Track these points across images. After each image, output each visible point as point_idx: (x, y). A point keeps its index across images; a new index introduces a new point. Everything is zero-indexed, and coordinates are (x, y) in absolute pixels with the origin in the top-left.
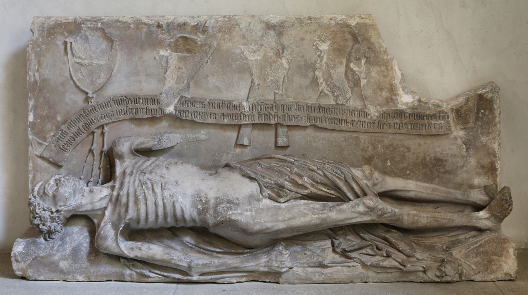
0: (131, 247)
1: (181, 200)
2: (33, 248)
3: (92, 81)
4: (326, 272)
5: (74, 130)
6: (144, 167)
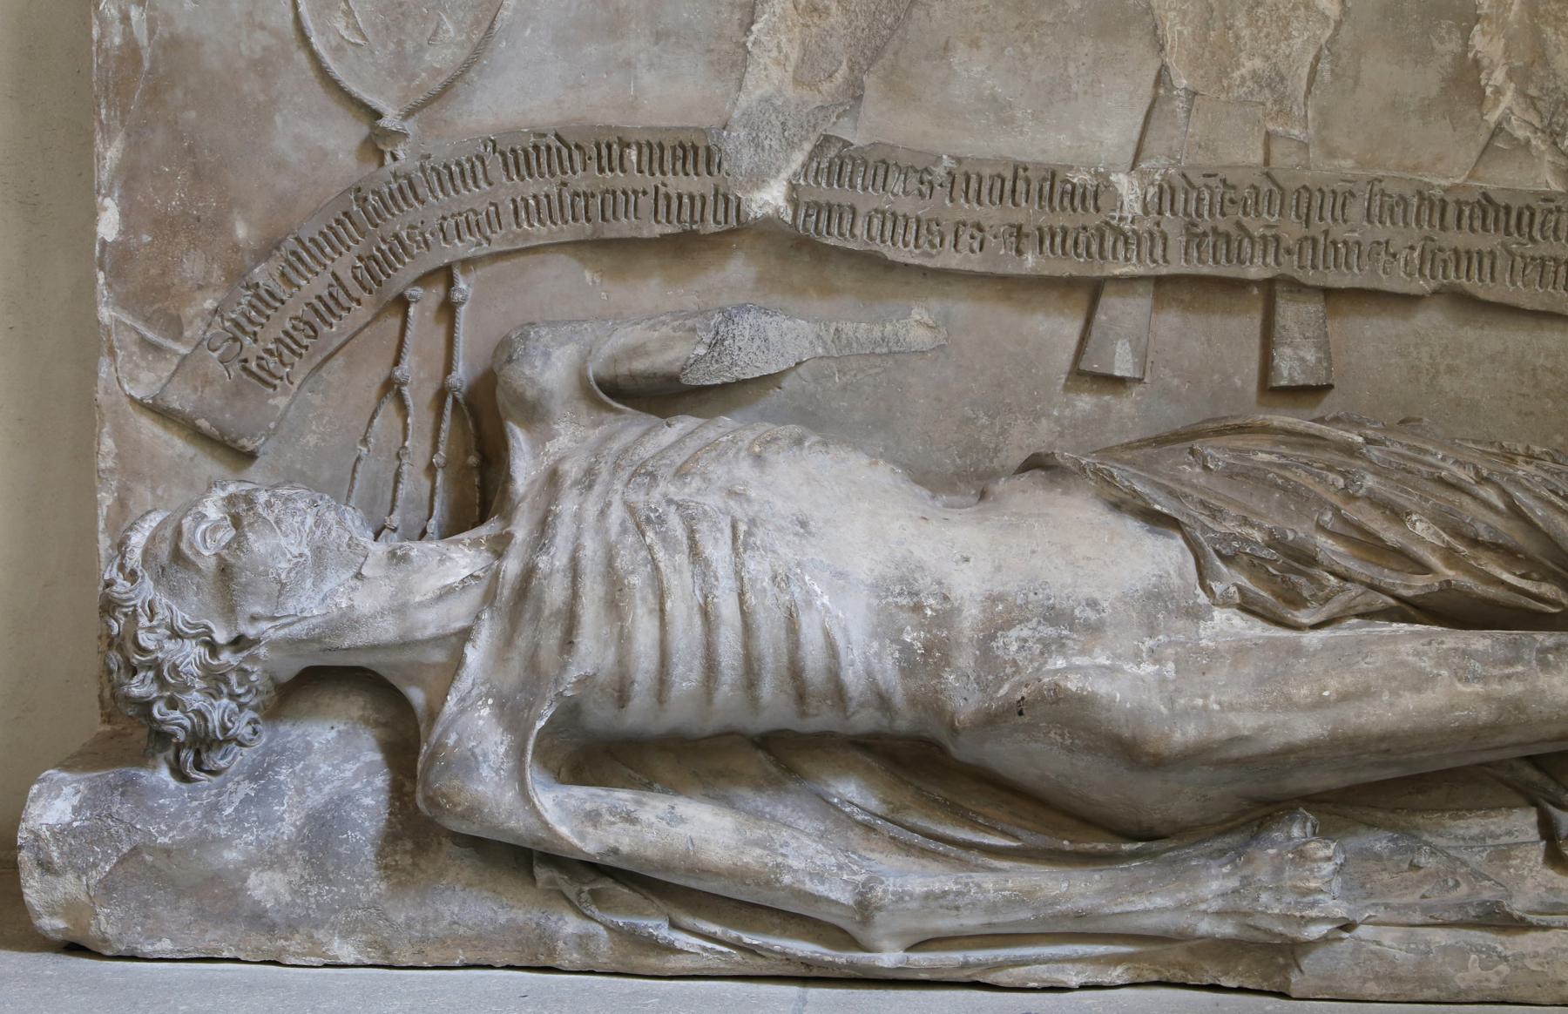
0: (588, 806)
1: (826, 599)
2: (122, 808)
3: (400, 55)
4: (1518, 949)
5: (315, 286)
6: (648, 450)
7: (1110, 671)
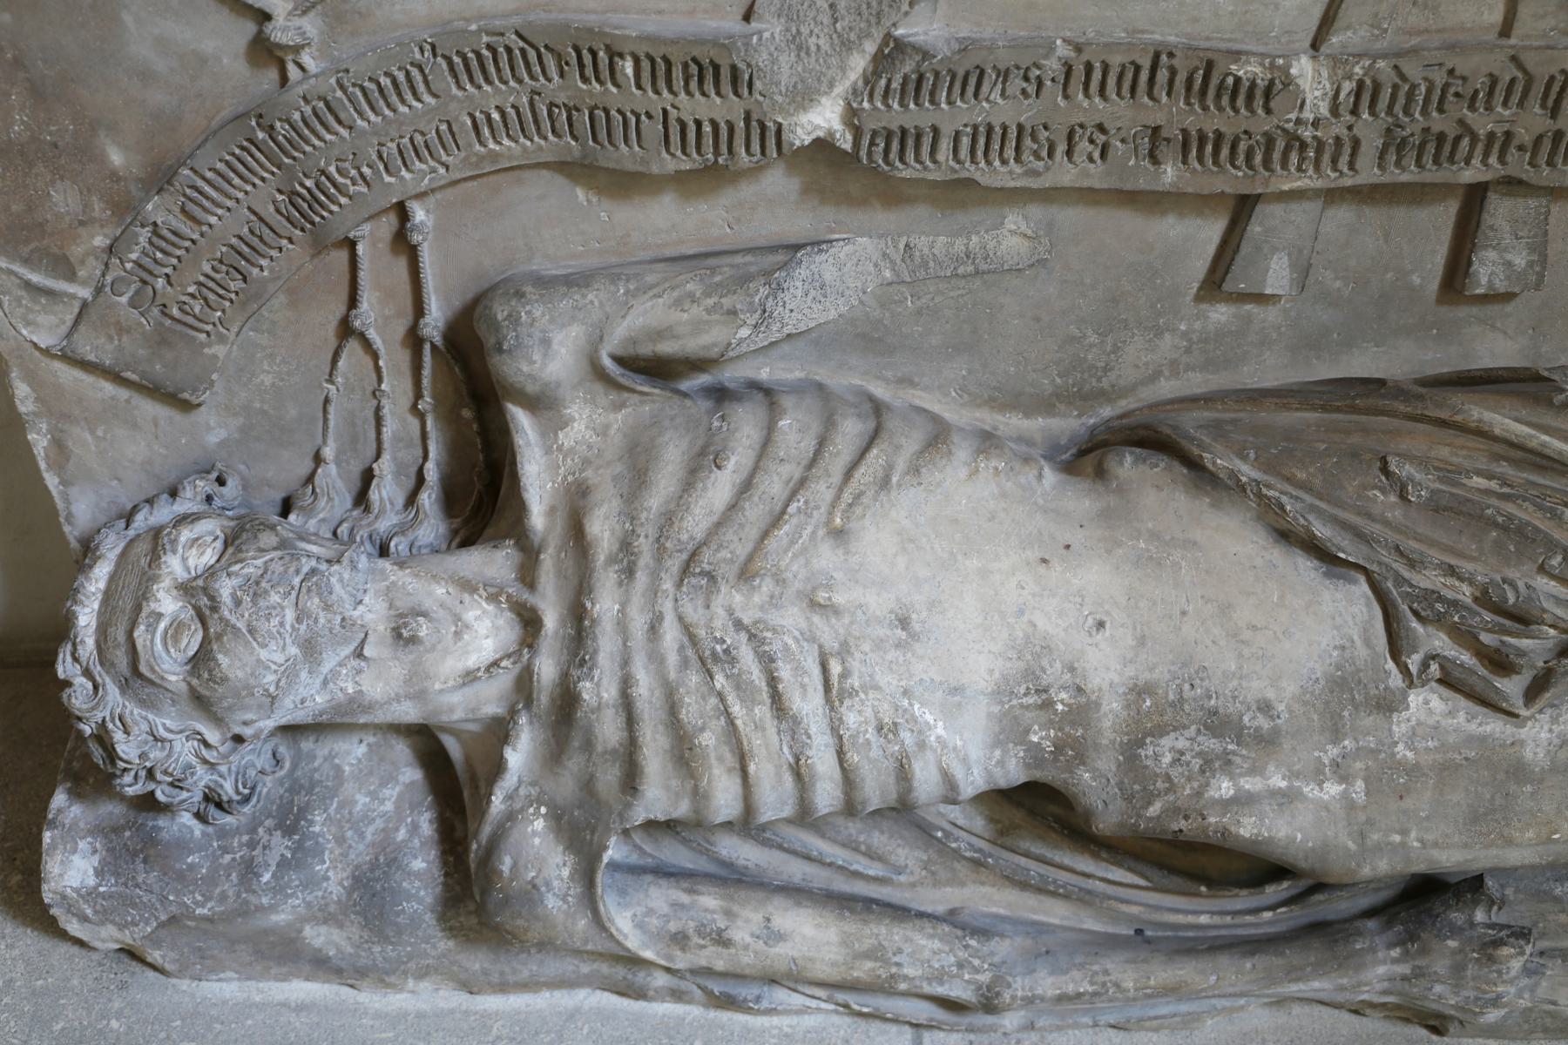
0: (673, 927)
1: (940, 731)
5: (226, 223)
6: (696, 523)
7: (1287, 798)
